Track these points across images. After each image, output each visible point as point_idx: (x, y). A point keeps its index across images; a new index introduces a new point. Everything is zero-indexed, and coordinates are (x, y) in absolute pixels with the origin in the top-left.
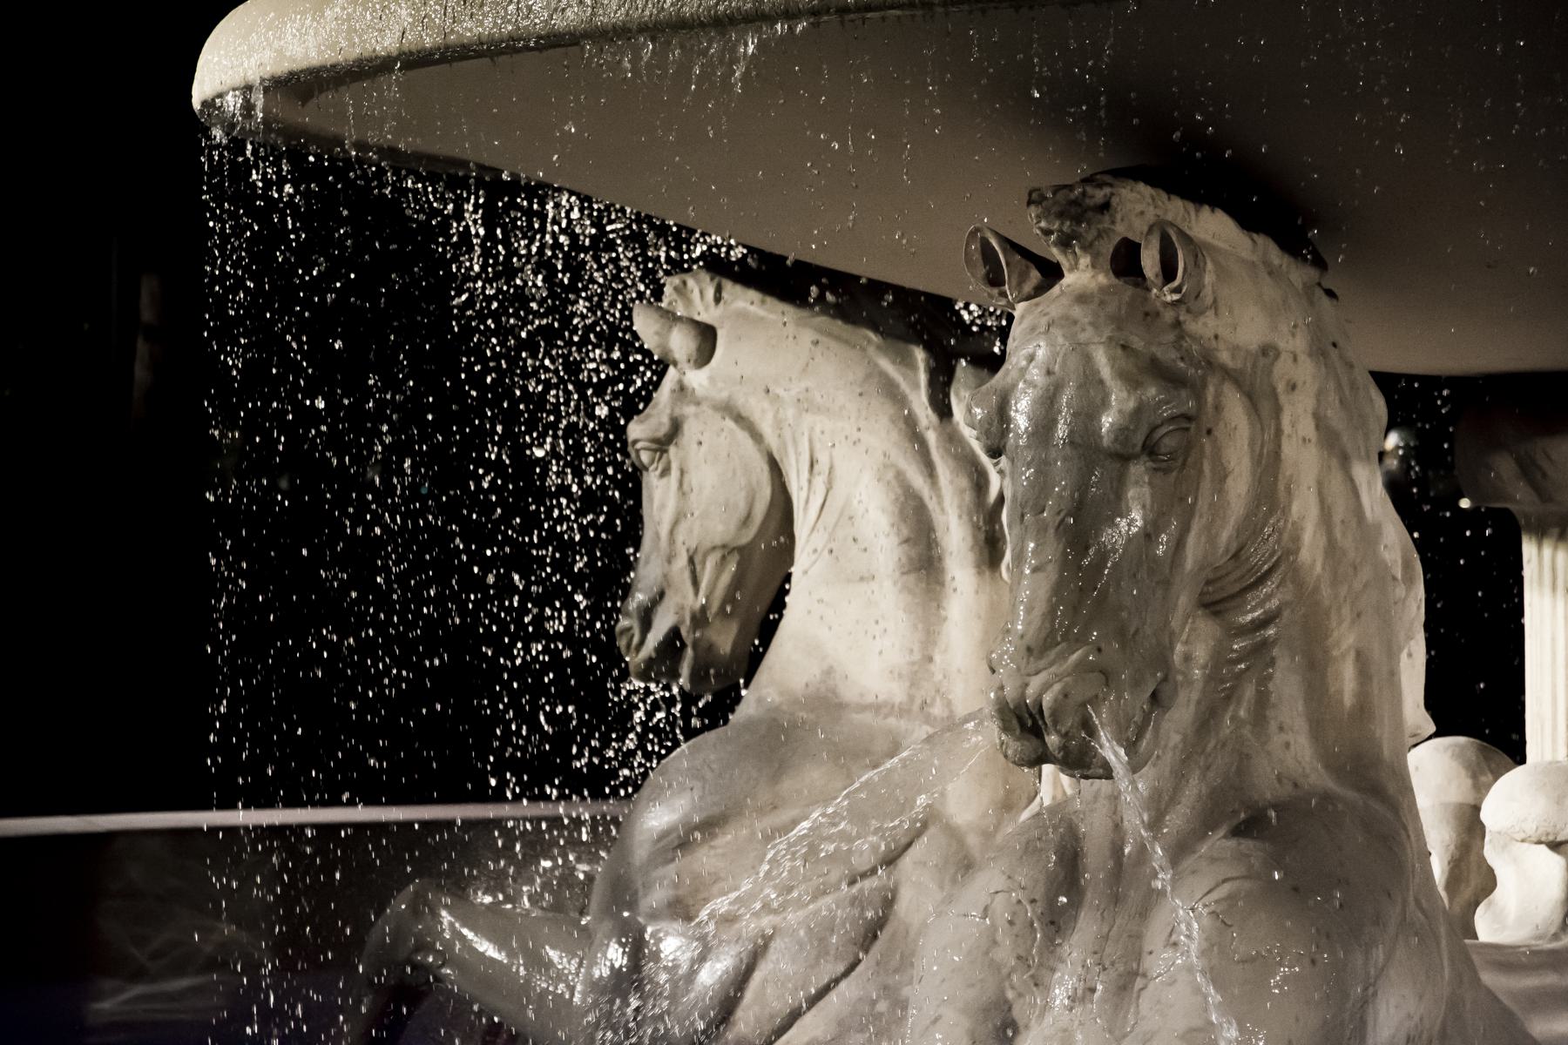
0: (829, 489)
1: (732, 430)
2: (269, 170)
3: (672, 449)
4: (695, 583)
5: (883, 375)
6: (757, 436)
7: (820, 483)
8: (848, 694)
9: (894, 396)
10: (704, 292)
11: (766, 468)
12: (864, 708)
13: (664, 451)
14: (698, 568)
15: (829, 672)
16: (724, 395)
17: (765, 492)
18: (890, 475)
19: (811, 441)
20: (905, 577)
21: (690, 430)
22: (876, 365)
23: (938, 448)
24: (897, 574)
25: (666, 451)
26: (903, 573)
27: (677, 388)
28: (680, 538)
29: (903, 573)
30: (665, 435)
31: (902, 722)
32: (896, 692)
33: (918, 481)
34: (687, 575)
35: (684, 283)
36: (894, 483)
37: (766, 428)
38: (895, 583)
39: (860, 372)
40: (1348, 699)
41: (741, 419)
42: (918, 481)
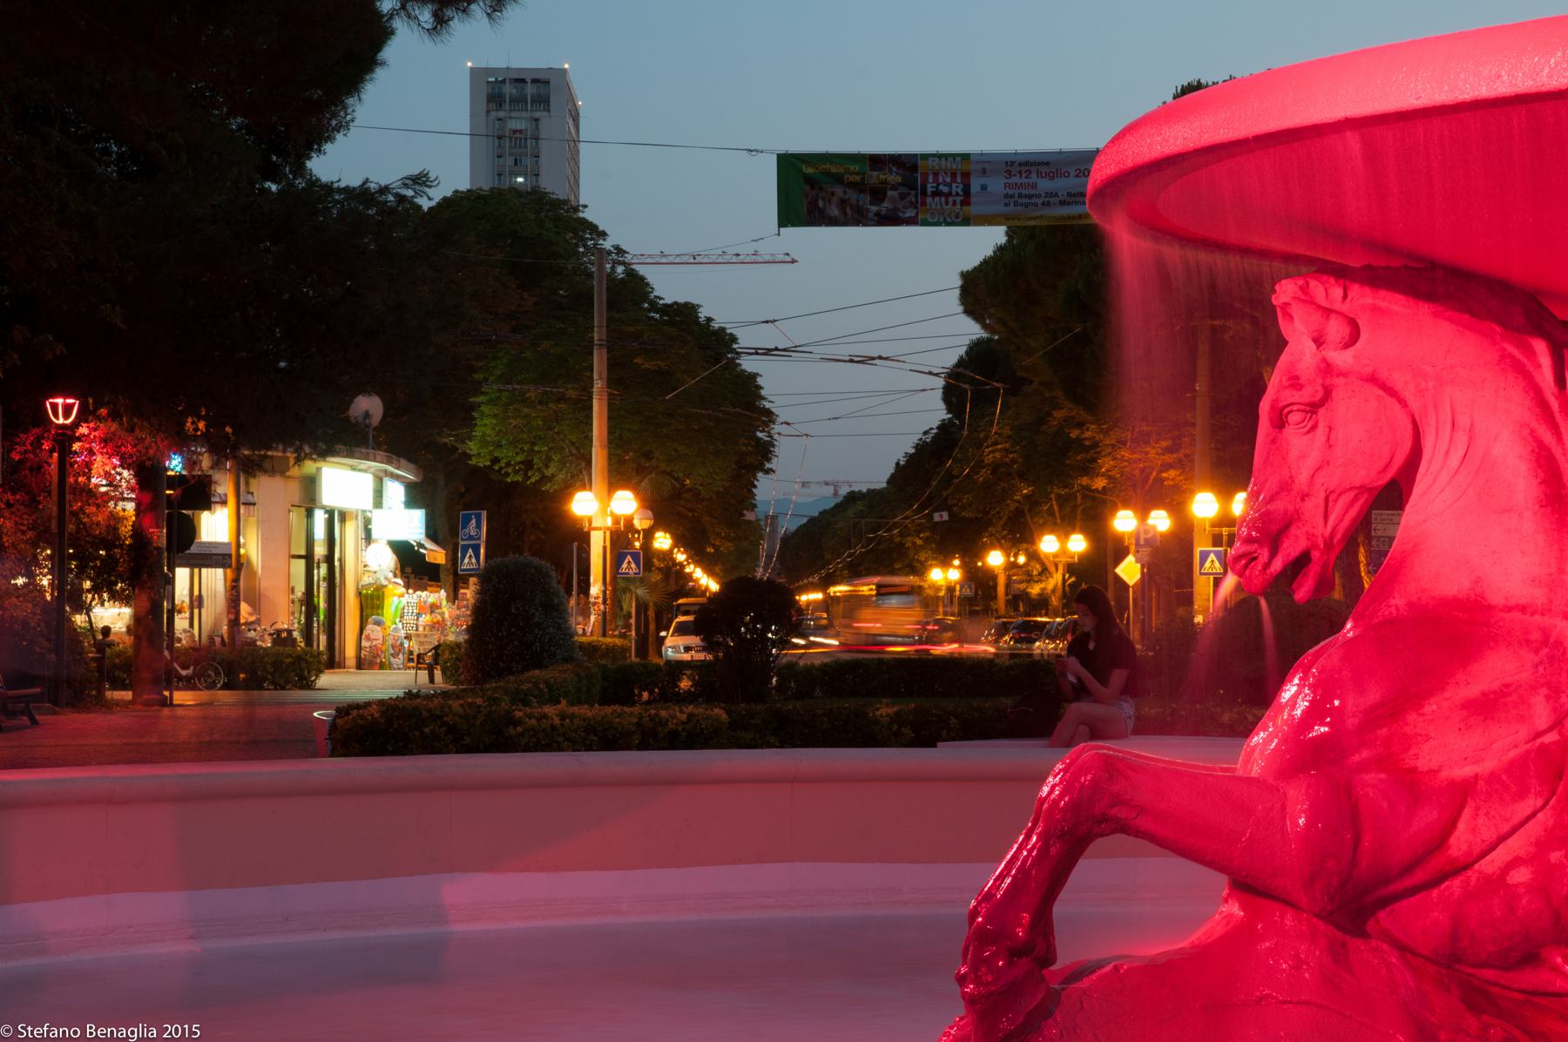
0: (1471, 438)
1: (1379, 396)
2: (1401, 225)
3: (1321, 411)
4: (1326, 518)
5: (1511, 356)
6: (1403, 403)
7: (1461, 440)
8: (1496, 598)
9: (1520, 370)
10: (1329, 291)
11: (1410, 426)
12: (1510, 609)
13: (1314, 412)
14: (1330, 504)
15: (1478, 580)
16: (1369, 370)
17: (1406, 446)
18: (1526, 432)
19: (1451, 403)
20: (1543, 509)
21: (1339, 395)
22: (1505, 350)
23: (1560, 412)
24: (1537, 507)
25: (1316, 413)
26: (1541, 506)
27: (1323, 366)
28: (1319, 480)
29: (1541, 506)
30: (1319, 400)
31: (1546, 619)
32: (1538, 596)
33: (1547, 437)
34: (1321, 510)
35: (1307, 283)
36: (1530, 437)
37: (1409, 395)
38: (1535, 513)
39: (1493, 355)
40: (1075, 681)
41: (1391, 392)
42: (1547, 437)
